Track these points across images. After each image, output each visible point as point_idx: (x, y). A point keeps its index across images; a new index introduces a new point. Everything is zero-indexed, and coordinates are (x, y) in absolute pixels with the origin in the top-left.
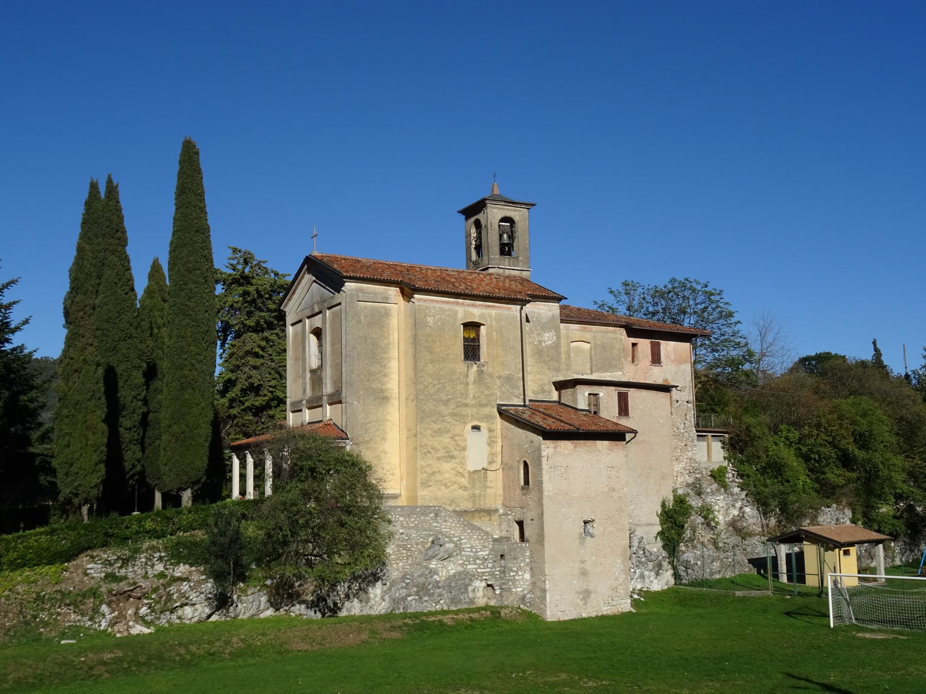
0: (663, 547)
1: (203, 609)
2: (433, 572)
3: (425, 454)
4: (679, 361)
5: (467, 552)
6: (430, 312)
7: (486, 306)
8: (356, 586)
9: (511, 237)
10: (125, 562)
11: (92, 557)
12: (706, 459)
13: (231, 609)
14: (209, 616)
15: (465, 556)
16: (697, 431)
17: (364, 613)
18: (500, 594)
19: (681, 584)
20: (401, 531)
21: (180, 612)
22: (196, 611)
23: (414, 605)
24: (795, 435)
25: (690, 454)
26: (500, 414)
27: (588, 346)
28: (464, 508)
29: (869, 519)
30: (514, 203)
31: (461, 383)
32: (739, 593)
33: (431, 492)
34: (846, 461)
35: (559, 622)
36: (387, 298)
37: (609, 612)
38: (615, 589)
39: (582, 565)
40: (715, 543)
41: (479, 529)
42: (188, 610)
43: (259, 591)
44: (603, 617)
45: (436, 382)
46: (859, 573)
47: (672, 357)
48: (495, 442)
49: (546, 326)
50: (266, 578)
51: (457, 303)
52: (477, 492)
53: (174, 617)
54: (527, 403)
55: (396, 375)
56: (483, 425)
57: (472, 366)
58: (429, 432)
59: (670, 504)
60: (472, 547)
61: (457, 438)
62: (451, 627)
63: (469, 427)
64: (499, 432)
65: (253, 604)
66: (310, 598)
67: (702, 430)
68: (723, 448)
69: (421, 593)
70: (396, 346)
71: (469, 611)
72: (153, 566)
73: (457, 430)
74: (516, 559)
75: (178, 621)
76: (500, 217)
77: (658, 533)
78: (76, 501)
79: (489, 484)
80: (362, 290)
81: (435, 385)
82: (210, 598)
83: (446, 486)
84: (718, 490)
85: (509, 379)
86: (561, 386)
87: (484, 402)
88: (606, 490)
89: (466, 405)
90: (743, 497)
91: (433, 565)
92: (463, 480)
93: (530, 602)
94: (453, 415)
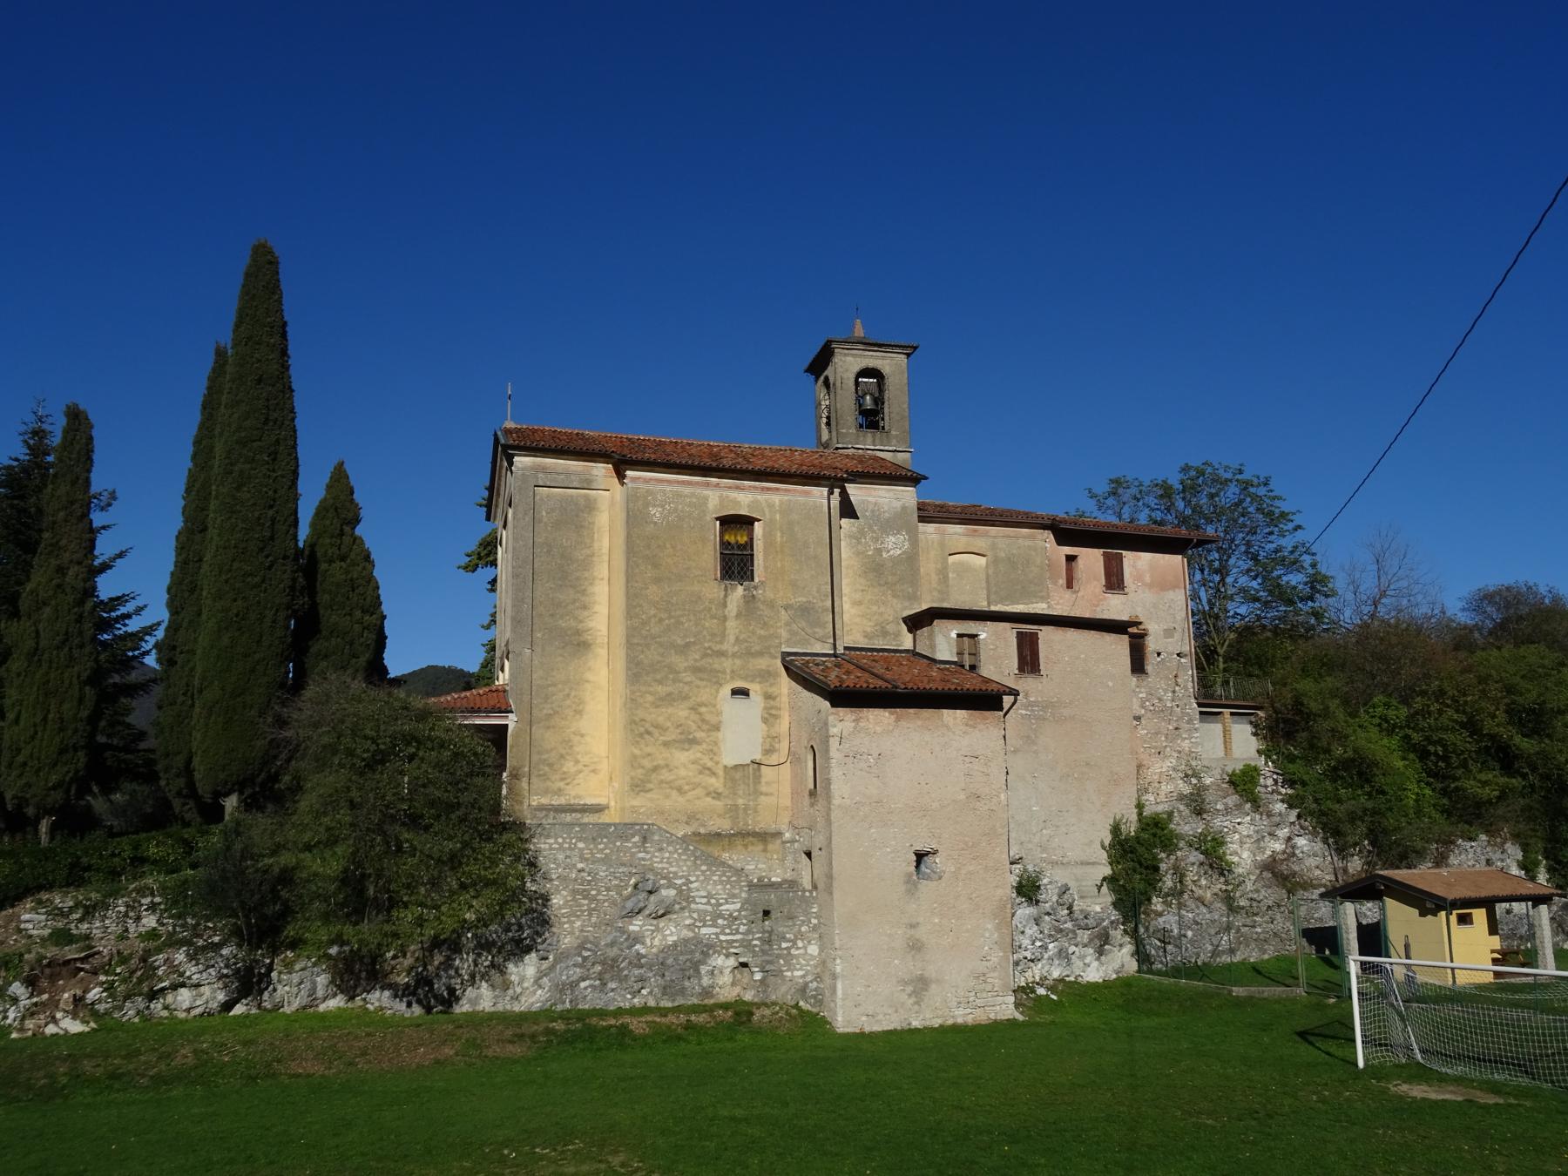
0: (1115, 905)
1: (213, 995)
2: (637, 939)
3: (641, 735)
4: (1161, 585)
5: (701, 905)
6: (655, 499)
7: (763, 489)
8: (486, 959)
9: (879, 401)
10: (89, 912)
11: (40, 902)
12: (1221, 754)
13: (266, 995)
14: (227, 1006)
15: (697, 911)
16: (1199, 705)
17: (500, 1008)
18: (762, 981)
19: (1150, 972)
20: (580, 866)
21: (170, 998)
22: (196, 994)
23: (590, 997)
24: (1400, 713)
25: (1186, 744)
26: (787, 669)
27: (982, 561)
28: (715, 829)
29: (1559, 862)
30: (880, 346)
31: (713, 617)
32: (1238, 991)
33: (651, 800)
34: (1505, 758)
35: (862, 1035)
36: (589, 481)
37: (970, 1020)
38: (981, 977)
39: (912, 932)
40: (1228, 899)
41: (723, 864)
42: (184, 996)
43: (315, 965)
44: (956, 1028)
45: (664, 615)
46: (1495, 961)
47: (1148, 579)
48: (776, 717)
49: (889, 525)
50: (331, 943)
51: (708, 484)
52: (740, 801)
53: (156, 1006)
54: (840, 650)
55: (603, 607)
56: (754, 688)
57: (734, 588)
58: (650, 698)
59: (1131, 828)
60: (709, 896)
61: (703, 709)
62: (644, 1037)
63: (726, 690)
64: (785, 699)
65: (301, 986)
66: (403, 979)
67: (1209, 704)
68: (1255, 734)
69: (607, 976)
70: (606, 558)
71: (696, 1009)
72: (138, 919)
73: (704, 695)
74: (791, 918)
75: (165, 1013)
76: (856, 369)
77: (1104, 879)
78: (30, 811)
79: (764, 789)
80: (544, 470)
81: (661, 620)
82: (226, 976)
83: (680, 790)
84: (1238, 807)
85: (805, 611)
86: (916, 622)
87: (757, 648)
88: (962, 797)
89: (722, 654)
90: (1293, 818)
91: (635, 926)
92: (713, 780)
93: (815, 997)
94: (696, 670)
